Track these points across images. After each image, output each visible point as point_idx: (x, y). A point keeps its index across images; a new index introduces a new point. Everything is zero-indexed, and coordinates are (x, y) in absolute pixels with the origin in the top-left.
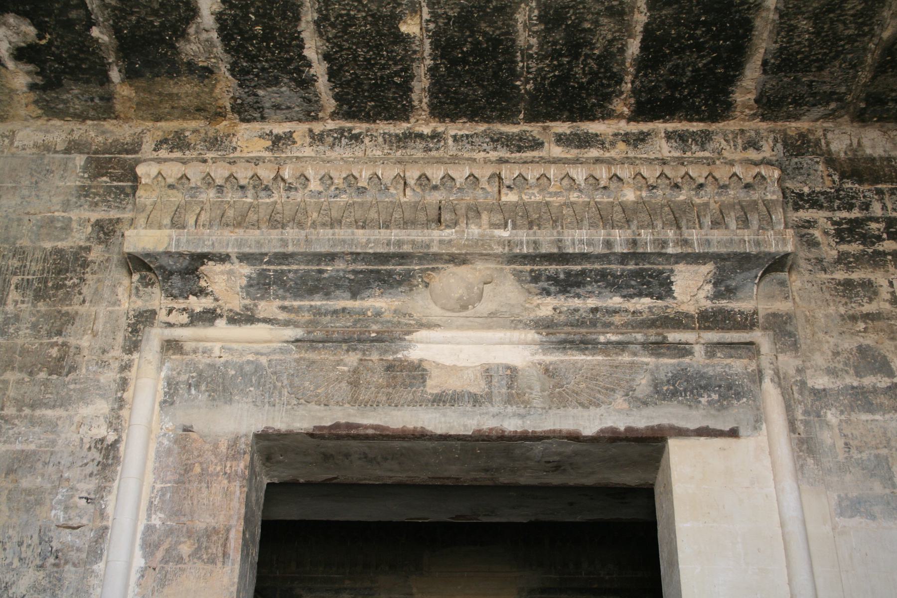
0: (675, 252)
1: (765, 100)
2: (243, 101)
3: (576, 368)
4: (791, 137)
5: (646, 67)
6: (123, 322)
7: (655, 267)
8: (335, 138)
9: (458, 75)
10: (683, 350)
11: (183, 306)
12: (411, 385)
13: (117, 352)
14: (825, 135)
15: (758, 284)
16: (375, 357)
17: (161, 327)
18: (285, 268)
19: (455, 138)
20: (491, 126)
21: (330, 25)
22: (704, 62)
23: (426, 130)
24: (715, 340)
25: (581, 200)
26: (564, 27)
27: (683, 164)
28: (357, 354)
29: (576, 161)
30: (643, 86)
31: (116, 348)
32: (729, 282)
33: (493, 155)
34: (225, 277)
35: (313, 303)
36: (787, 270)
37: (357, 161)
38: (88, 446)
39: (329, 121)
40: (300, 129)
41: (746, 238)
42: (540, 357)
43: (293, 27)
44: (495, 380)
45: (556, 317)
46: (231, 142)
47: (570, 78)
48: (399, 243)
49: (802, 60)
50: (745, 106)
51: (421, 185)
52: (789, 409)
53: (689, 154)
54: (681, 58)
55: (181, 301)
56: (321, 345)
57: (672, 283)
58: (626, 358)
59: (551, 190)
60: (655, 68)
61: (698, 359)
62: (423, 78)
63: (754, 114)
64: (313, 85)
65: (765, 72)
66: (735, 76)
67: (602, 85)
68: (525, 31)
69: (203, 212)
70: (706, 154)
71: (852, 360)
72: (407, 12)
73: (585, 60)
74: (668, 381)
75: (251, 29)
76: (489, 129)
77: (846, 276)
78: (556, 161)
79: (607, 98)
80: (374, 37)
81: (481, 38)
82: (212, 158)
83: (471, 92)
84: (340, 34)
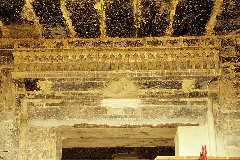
0: (183, 76)
1: (217, 28)
2: (45, 32)
3: (152, 108)
4: (224, 40)
5: (177, 19)
6: (15, 98)
7: (177, 80)
8: (77, 43)
9: (115, 23)
10: (184, 103)
11: (32, 93)
12: (103, 113)
13: (14, 106)
14: (236, 39)
15: (209, 85)
16: (92, 106)
17: (27, 99)
18: (63, 82)
19: (115, 43)
20: (127, 39)
21: (71, 7)
22: (197, 17)
23: (106, 41)
24: (194, 100)
25: (154, 61)
26: (149, 6)
27: (188, 50)
28: (86, 106)
29: (154, 50)
30: (176, 25)
31: (13, 105)
32: (200, 84)
33: (127, 48)
34: (45, 85)
35: (72, 92)
36: (218, 80)
37: (84, 50)
38: (8, 131)
39: (74, 38)
40: (65, 41)
41: (206, 72)
42: (141, 106)
43: (58, 8)
44: (127, 112)
45: (146, 94)
46: (43, 45)
47: (152, 23)
48: (98, 75)
49: (230, 15)
50: (210, 31)
51: (104, 57)
52: (215, 118)
53: (190, 46)
54: (189, 16)
55: (32, 92)
56: (75, 103)
57: (182, 85)
58: (167, 105)
59: (145, 58)
60: (180, 20)
61: (188, 106)
62: (103, 24)
63: (213, 33)
64: (67, 27)
65: (217, 19)
66: (207, 21)
67: (163, 25)
68: (136, 8)
69: (36, 66)
70: (196, 46)
71: (236, 105)
72: (96, 2)
73: (157, 17)
74: (179, 112)
75: (44, 8)
76: (126, 40)
77: (237, 82)
78: (147, 50)
79: (164, 29)
80: (86, 11)
81: (122, 11)
82: (37, 50)
83: (119, 28)
84: (75, 10)
